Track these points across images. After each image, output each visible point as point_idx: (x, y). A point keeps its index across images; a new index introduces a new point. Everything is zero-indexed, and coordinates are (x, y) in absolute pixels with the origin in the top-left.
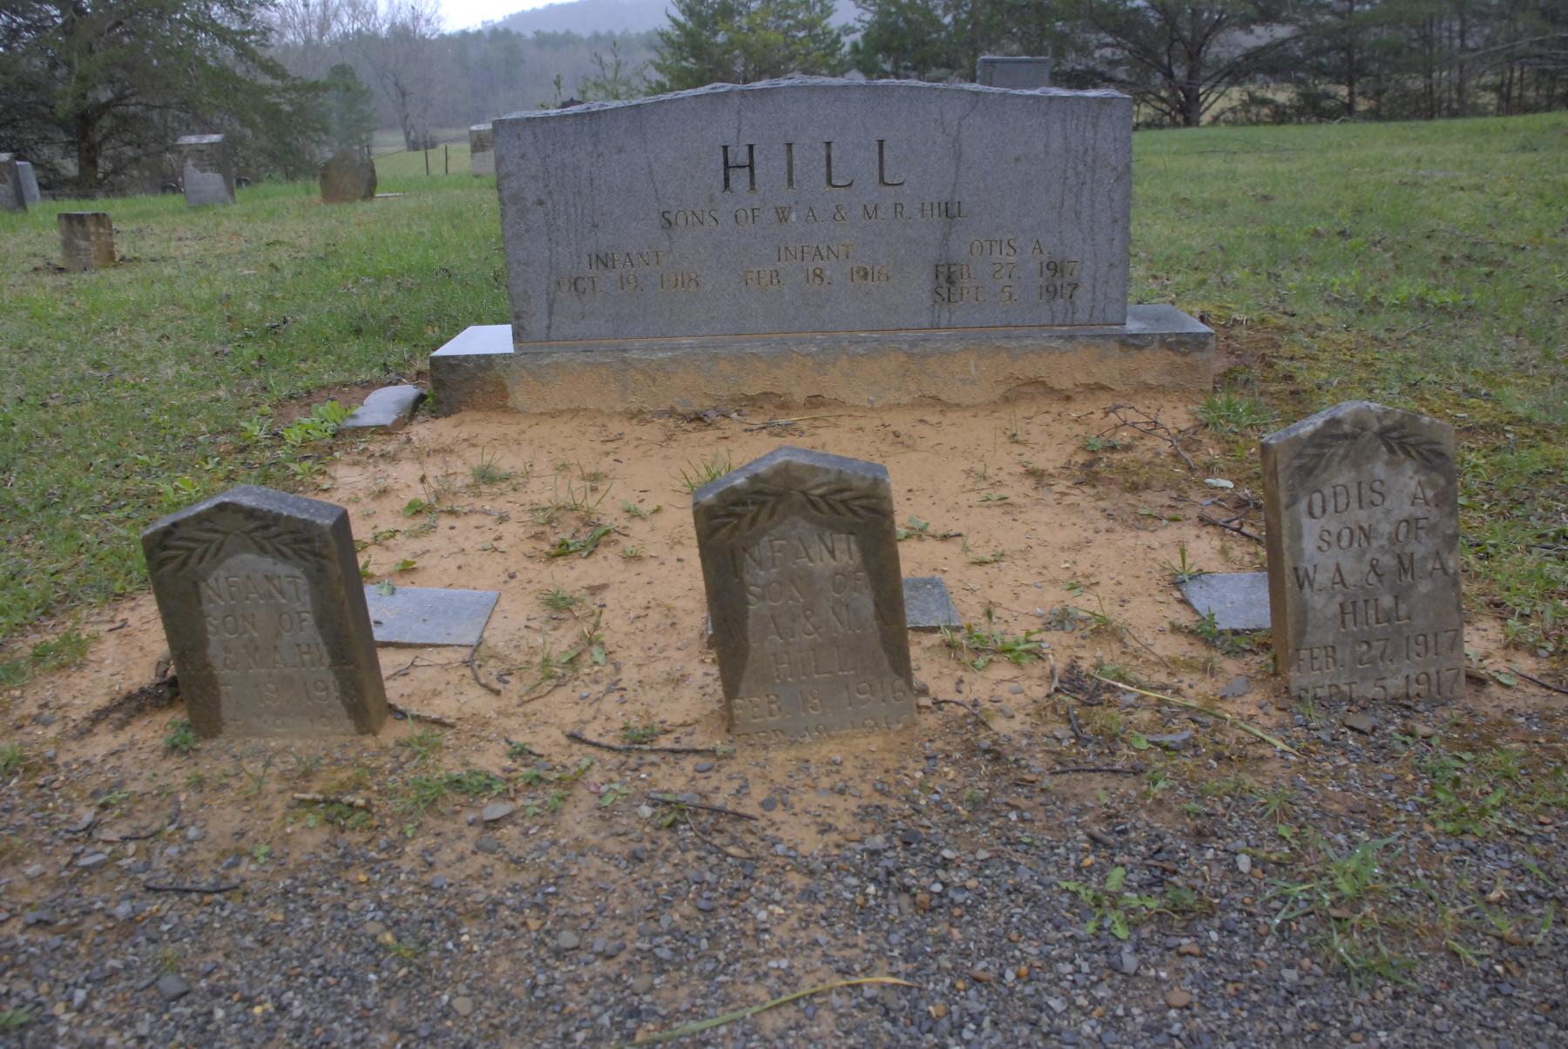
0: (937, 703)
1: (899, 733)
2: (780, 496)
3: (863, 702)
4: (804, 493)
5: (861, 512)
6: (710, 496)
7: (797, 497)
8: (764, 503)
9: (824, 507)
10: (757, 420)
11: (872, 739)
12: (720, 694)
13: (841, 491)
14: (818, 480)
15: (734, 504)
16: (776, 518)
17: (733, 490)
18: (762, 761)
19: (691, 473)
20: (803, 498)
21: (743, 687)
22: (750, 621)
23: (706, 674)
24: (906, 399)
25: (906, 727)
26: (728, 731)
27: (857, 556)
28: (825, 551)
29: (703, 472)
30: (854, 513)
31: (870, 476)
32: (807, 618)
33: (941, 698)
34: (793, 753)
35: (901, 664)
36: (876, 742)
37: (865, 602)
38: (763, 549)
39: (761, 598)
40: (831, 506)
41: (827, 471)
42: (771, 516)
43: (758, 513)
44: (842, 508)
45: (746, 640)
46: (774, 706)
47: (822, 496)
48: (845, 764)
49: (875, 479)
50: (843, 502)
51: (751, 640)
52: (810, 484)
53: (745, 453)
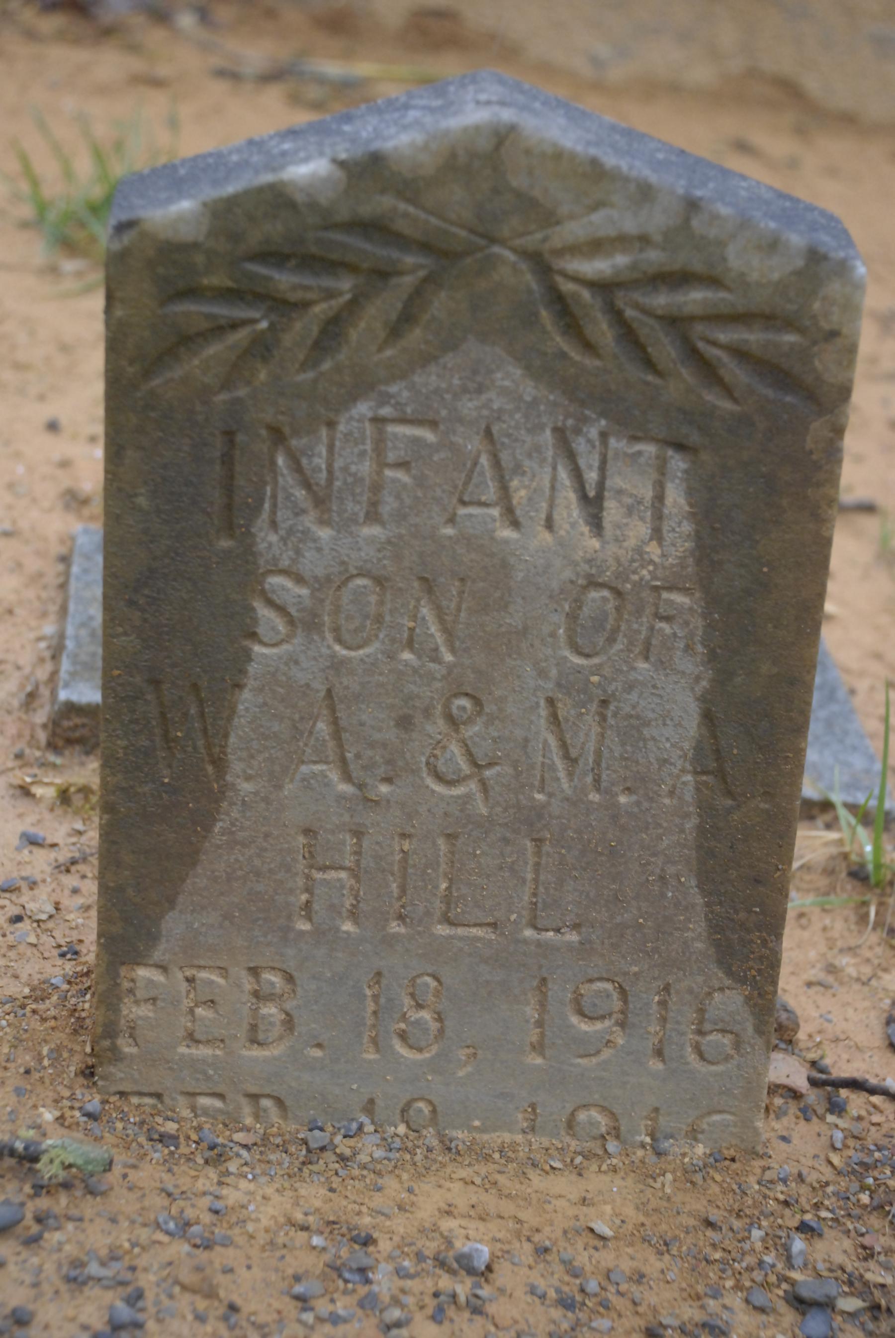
0: (831, 1087)
1: (690, 1176)
2: (444, 256)
3: (587, 1048)
4: (540, 264)
5: (734, 372)
6: (186, 205)
7: (511, 272)
8: (383, 274)
9: (603, 331)
10: (255, 52)
11: (595, 1181)
12: (86, 929)
13: (681, 279)
14: (600, 222)
15: (274, 256)
16: (416, 336)
17: (277, 199)
18: (198, 1211)
19: (47, 168)
20: (530, 279)
21: (173, 925)
22: (246, 700)
23: (33, 842)
24: (701, 74)
25: (717, 1159)
26: (88, 1073)
27: (681, 532)
28: (568, 495)
29: (84, 166)
30: (708, 370)
31: (796, 240)
32: (452, 721)
33: (843, 1067)
34: (313, 1194)
35: (747, 941)
36: (611, 1199)
37: (672, 703)
38: (346, 446)
39: (306, 623)
40: (628, 334)
41: (645, 193)
42: (395, 332)
43: (355, 304)
44: (665, 349)
45: (220, 763)
46: (270, 1010)
47: (603, 288)
48: (504, 1275)
49: (815, 256)
50: (675, 322)
51: (237, 766)
52: (574, 230)
53: (215, 127)
